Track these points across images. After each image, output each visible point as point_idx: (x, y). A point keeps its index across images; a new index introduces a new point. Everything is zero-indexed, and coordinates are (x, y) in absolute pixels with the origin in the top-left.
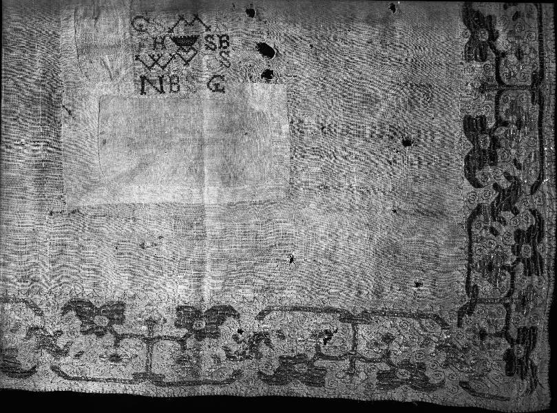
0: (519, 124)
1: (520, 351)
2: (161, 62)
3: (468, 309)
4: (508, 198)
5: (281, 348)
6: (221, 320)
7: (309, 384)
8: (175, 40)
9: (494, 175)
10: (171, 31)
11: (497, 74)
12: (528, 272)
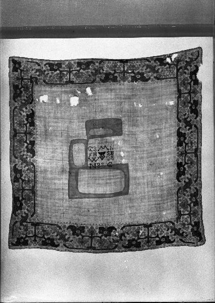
2: (96, 160)
5: (128, 237)
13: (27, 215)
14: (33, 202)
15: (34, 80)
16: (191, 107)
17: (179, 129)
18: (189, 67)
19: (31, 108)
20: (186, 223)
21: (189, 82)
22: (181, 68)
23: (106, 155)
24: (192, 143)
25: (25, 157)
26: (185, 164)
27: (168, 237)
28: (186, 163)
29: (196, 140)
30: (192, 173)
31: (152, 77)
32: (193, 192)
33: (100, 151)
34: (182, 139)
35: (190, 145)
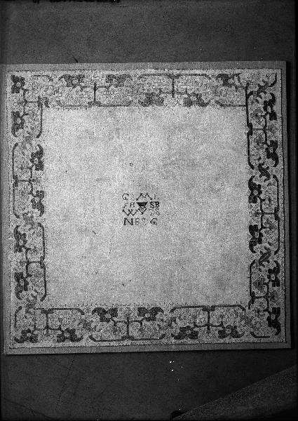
0: (271, 228)
1: (273, 317)
2: (133, 213)
3: (252, 301)
4: (265, 257)
5: (180, 324)
6: (180, 334)
7: (191, 338)
8: (138, 203)
9: (95, 319)
10: (137, 199)
11: (261, 208)
12: (274, 286)
13: (35, 297)
14: (42, 279)
15: (43, 102)
16: (267, 149)
17: (251, 179)
18: (262, 94)
19: (90, 314)
20: (262, 309)
21: (263, 114)
22: (251, 93)
23: (148, 206)
24: (270, 200)
25: (29, 215)
26: (261, 229)
27: (235, 327)
28: (263, 227)
29: (276, 196)
30: (271, 242)
31: (213, 102)
32: (272, 268)
33: (140, 201)
34: (256, 193)
35: (267, 202)
